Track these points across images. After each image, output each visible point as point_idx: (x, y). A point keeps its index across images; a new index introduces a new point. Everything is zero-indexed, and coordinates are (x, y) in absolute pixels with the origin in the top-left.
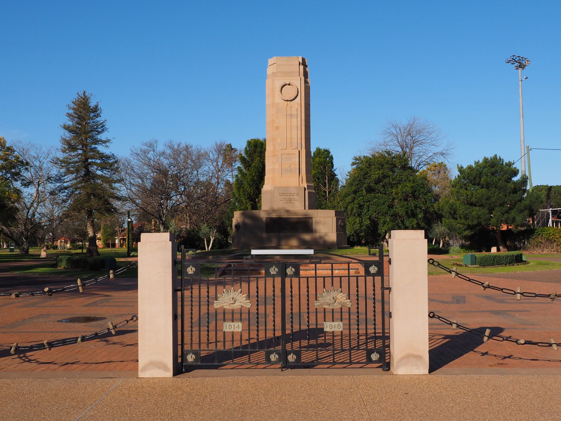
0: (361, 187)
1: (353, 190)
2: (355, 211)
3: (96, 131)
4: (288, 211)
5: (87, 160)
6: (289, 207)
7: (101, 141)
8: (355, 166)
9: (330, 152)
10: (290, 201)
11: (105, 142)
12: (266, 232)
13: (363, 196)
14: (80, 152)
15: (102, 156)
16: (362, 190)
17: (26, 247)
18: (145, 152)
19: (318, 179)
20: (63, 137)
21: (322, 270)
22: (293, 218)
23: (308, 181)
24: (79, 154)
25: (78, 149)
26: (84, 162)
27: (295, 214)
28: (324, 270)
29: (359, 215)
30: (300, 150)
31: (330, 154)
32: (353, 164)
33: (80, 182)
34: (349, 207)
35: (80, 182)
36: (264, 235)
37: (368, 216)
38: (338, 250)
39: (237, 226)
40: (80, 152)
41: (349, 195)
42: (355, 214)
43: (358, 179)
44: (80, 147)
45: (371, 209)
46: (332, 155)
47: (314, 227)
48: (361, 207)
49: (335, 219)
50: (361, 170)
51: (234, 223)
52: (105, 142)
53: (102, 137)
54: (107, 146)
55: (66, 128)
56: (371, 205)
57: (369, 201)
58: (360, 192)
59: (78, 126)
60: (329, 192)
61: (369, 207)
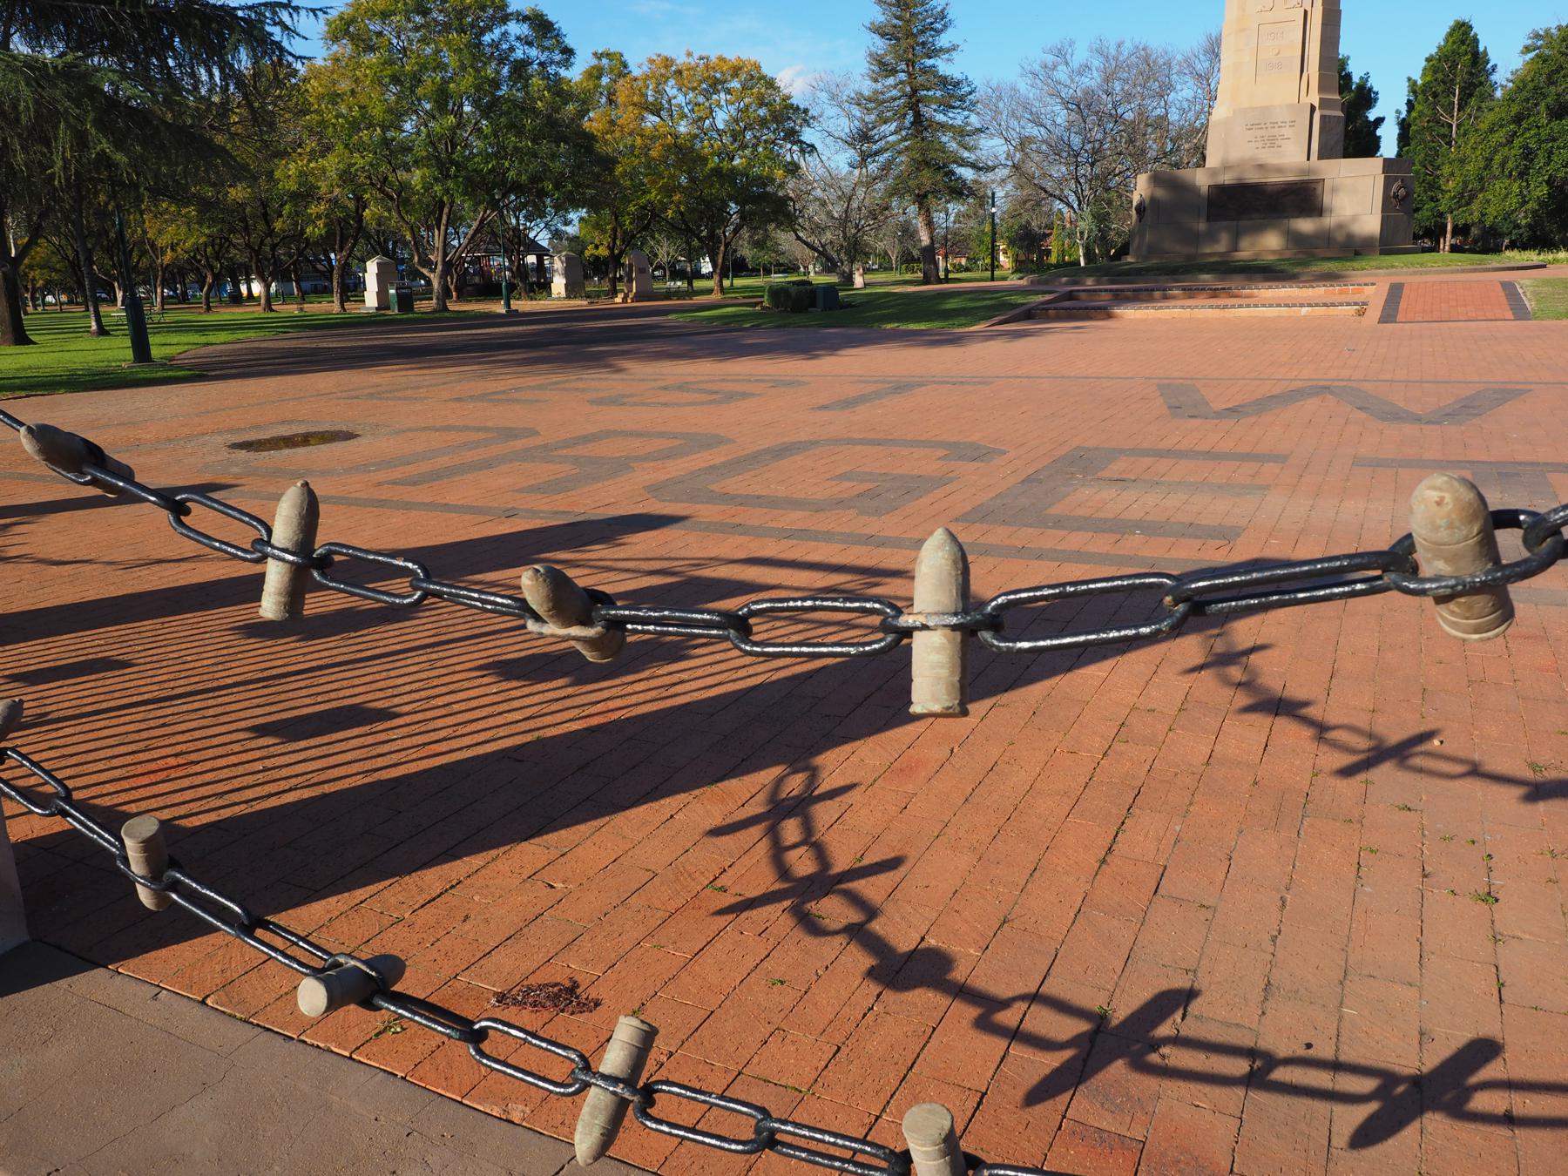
0: (1536, 105)
1: (1512, 114)
2: (1510, 165)
3: (932, 29)
4: (1261, 167)
5: (915, 91)
6: (1269, 157)
7: (941, 50)
8: (1532, 55)
9: (1471, 28)
10: (1272, 142)
11: (948, 51)
12: (1208, 221)
13: (1538, 127)
14: (903, 76)
15: (944, 81)
16: (1538, 113)
17: (847, 270)
18: (1049, 69)
19: (1435, 95)
20: (872, 49)
21: (1264, 306)
22: (1276, 184)
23: (1321, 89)
24: (901, 82)
25: (897, 72)
26: (910, 98)
27: (1279, 170)
28: (1271, 306)
29: (1522, 175)
30: (1309, 9)
31: (1472, 33)
32: (1527, 49)
33: (904, 139)
34: (1498, 158)
35: (904, 139)
36: (1202, 226)
37: (1546, 178)
38: (1383, 257)
39: (1141, 209)
40: (903, 76)
41: (1502, 126)
42: (1510, 173)
43: (1531, 86)
44: (904, 67)
45: (1555, 159)
46: (1476, 35)
47: (1326, 200)
48: (1528, 155)
49: (1381, 179)
50: (1545, 61)
51: (1136, 199)
52: (948, 51)
53: (943, 41)
54: (948, 60)
55: (879, 31)
56: (1558, 148)
57: (1554, 140)
58: (1532, 119)
59: (895, 21)
60: (1458, 126)
61: (1550, 153)
